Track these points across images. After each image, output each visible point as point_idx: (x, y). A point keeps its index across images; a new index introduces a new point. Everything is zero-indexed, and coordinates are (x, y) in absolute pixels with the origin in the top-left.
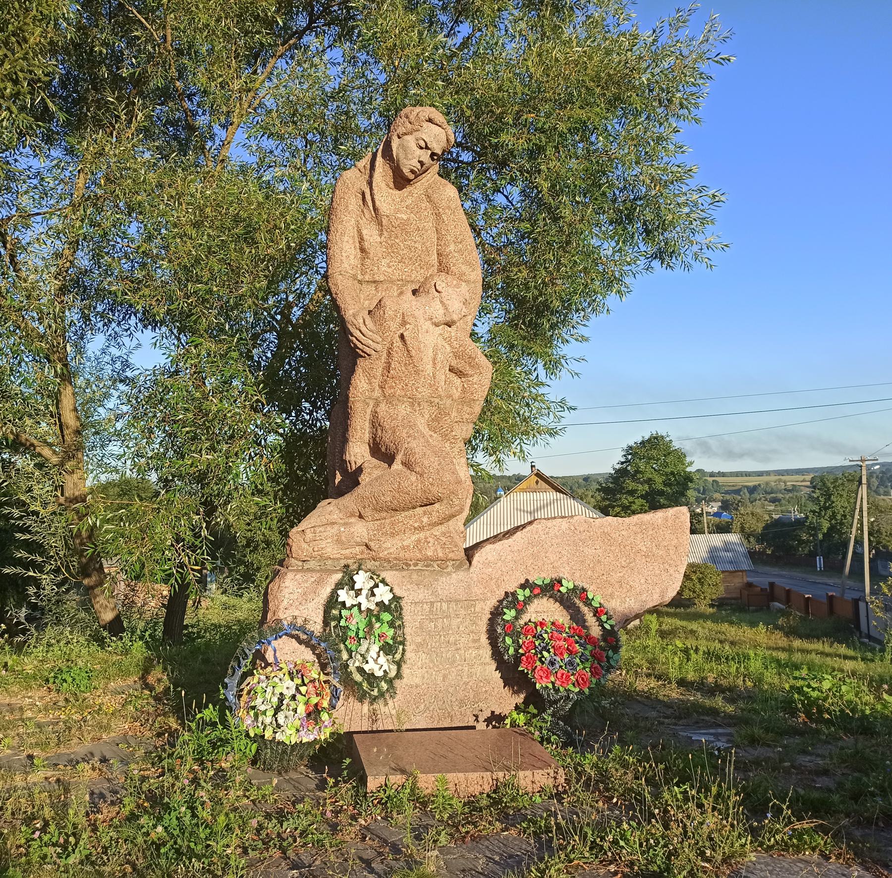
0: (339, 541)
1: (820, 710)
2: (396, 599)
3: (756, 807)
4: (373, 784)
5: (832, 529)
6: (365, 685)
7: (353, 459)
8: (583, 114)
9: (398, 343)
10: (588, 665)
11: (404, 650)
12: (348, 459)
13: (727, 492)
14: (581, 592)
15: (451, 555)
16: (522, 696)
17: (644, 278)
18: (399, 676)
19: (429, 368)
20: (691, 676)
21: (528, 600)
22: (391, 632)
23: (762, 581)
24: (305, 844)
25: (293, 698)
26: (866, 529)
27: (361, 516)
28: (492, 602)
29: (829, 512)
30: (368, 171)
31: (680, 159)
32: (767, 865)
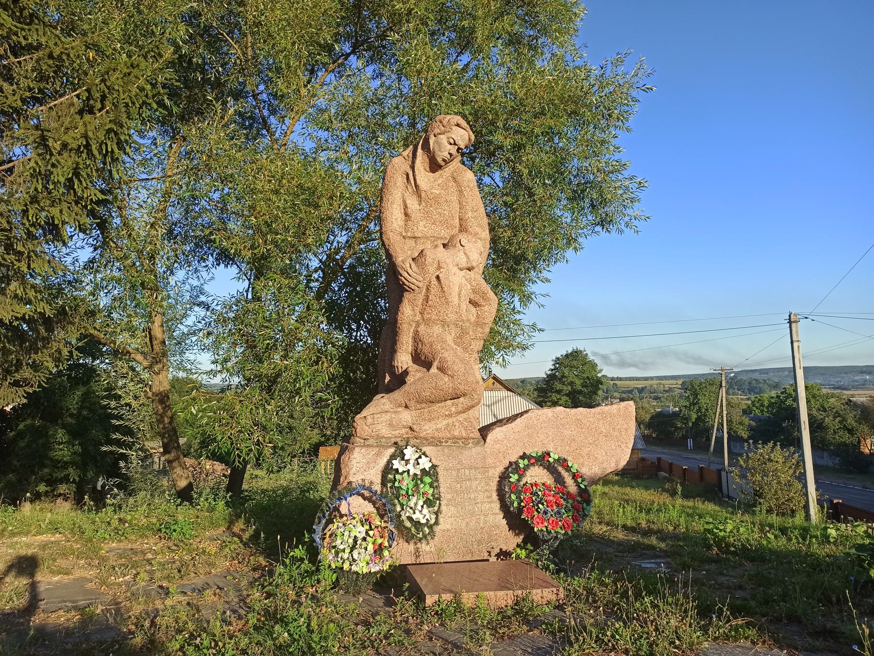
0: (391, 425)
1: (728, 545)
2: (434, 467)
3: (705, 612)
4: (430, 600)
5: (698, 419)
6: (413, 529)
7: (400, 365)
8: (552, 123)
9: (434, 282)
10: (570, 514)
11: (440, 504)
12: (396, 364)
13: (623, 392)
14: (563, 462)
15: (471, 435)
16: (522, 537)
17: (592, 238)
18: (437, 523)
19: (456, 300)
20: (629, 523)
21: (527, 468)
22: (431, 491)
23: (652, 457)
24: (389, 644)
25: (364, 539)
26: (725, 419)
27: (406, 407)
28: (500, 469)
29: (697, 407)
30: (411, 159)
31: (617, 156)
32: (717, 650)
